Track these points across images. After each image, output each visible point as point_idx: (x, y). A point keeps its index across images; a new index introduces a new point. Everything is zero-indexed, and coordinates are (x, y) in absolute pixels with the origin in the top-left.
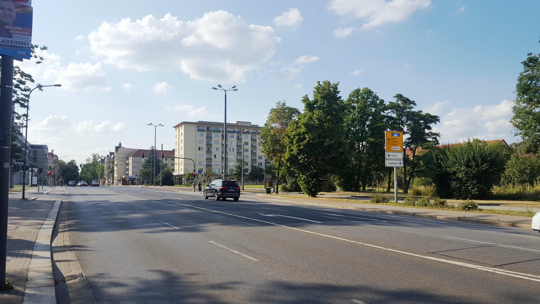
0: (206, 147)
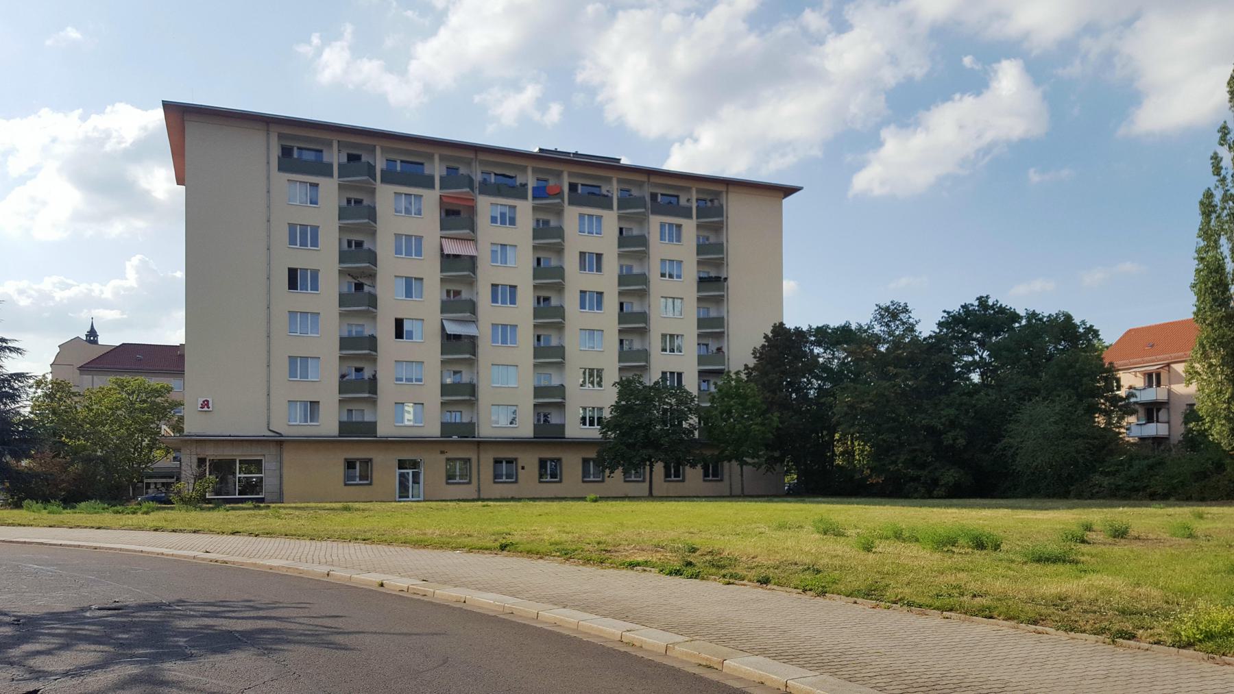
0: (340, 272)
